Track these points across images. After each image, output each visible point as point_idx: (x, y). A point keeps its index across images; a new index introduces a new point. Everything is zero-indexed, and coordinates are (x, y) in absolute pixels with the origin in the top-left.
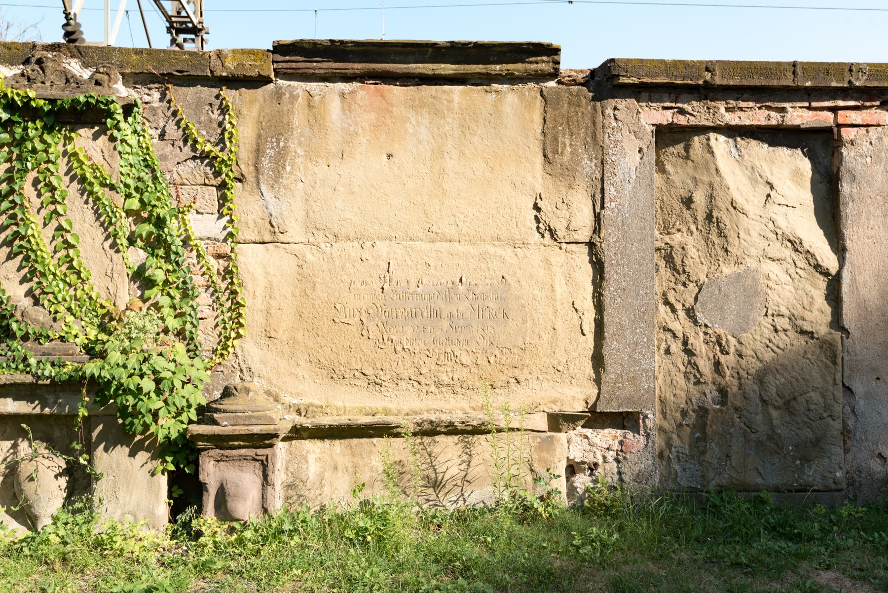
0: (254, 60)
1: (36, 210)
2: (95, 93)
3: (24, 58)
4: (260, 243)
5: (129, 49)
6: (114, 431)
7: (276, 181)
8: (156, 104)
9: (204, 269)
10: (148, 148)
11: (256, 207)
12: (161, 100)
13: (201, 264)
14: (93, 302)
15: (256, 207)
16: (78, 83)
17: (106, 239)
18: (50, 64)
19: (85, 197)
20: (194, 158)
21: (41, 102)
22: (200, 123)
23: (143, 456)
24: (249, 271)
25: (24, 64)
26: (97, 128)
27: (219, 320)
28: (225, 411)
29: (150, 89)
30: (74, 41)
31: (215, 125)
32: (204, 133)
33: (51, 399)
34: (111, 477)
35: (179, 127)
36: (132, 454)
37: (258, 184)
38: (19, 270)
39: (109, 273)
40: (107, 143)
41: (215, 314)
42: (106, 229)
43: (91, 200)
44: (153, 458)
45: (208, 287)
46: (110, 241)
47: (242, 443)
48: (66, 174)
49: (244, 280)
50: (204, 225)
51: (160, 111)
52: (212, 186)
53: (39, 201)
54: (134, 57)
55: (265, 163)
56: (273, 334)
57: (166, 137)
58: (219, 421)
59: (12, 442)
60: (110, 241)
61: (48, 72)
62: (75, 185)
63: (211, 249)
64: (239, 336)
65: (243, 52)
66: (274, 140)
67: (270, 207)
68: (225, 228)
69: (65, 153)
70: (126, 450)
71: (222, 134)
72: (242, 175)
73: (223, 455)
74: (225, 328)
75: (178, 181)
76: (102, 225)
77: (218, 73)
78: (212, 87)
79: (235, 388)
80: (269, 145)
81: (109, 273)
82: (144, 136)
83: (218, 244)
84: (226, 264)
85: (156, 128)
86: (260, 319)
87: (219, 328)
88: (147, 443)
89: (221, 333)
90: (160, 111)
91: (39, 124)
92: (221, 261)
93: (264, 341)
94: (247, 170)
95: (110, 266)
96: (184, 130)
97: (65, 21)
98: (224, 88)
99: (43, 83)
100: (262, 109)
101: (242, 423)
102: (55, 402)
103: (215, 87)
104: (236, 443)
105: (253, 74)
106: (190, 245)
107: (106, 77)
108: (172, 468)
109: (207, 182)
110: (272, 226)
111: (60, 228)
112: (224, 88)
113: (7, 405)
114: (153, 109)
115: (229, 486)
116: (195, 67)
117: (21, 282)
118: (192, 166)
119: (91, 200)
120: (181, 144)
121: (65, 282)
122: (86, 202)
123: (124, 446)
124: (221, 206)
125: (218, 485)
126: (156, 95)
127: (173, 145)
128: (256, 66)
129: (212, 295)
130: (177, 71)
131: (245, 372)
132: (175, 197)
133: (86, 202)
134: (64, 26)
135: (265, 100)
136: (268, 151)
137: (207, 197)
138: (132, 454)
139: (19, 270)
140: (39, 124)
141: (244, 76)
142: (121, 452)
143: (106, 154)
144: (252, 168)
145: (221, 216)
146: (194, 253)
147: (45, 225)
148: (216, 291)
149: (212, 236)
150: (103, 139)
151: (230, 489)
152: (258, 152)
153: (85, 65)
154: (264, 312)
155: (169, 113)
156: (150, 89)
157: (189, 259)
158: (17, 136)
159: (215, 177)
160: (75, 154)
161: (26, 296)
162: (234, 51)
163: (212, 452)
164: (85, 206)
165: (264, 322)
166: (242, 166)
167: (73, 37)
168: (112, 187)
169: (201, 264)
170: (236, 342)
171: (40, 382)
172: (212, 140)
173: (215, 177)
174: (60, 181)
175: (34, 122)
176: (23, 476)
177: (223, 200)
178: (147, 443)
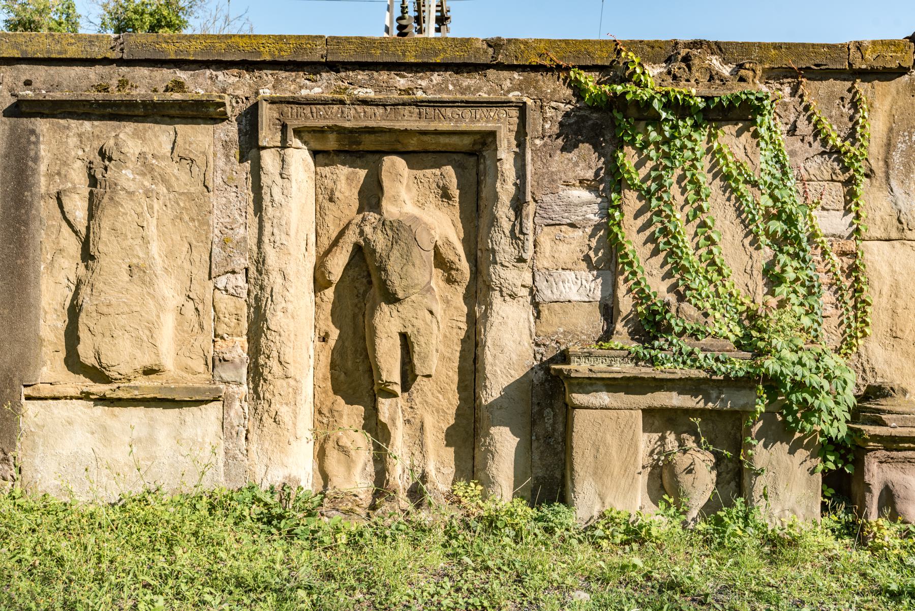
0: (894, 52)
1: (679, 207)
2: (738, 89)
3: (667, 56)
4: (886, 240)
5: (768, 44)
6: (773, 427)
7: (906, 176)
8: (787, 100)
9: (829, 266)
10: (780, 145)
11: (885, 204)
12: (793, 94)
13: (826, 262)
14: (733, 299)
15: (885, 204)
16: (723, 80)
17: (746, 236)
18: (696, 61)
19: (727, 194)
20: (822, 154)
21: (699, 100)
22: (831, 117)
23: (802, 454)
24: (875, 270)
25: (666, 62)
26: (740, 125)
27: (844, 318)
28: (890, 412)
29: (782, 84)
30: (405, 34)
31: (846, 119)
32: (835, 127)
33: (714, 394)
34: (771, 473)
35: (810, 122)
36: (792, 452)
37: (888, 178)
38: (662, 266)
39: (748, 270)
40: (750, 140)
41: (839, 312)
42: (746, 227)
43: (733, 197)
44: (813, 456)
45: (831, 285)
46: (750, 238)
47: (912, 445)
48: (709, 171)
49: (871, 278)
50: (830, 222)
51: (791, 107)
52: (839, 181)
53: (683, 198)
54: (773, 52)
55: (897, 158)
56: (899, 334)
57: (797, 133)
58: (887, 422)
59: (660, 434)
60: (750, 238)
61: (694, 69)
62: (718, 182)
63: (835, 246)
64: (865, 335)
65: (883, 43)
66: (906, 133)
67: (900, 203)
68: (851, 224)
69: (709, 150)
70: (787, 447)
71: (853, 129)
72: (871, 170)
73: (888, 457)
74: (849, 326)
75: (806, 177)
76: (743, 222)
77: (856, 66)
78: (845, 80)
79: (892, 388)
80: (901, 139)
81: (748, 270)
82: (775, 132)
83: (842, 241)
84: (851, 261)
85: (787, 124)
86: (885, 318)
87: (843, 327)
88: (806, 441)
89: (845, 332)
90: (791, 107)
91: (689, 122)
92: (844, 259)
93: (889, 341)
94: (878, 166)
95: (750, 263)
96: (815, 126)
97: (400, 15)
98: (858, 81)
99: (688, 80)
100: (894, 101)
101: (910, 424)
102: (718, 398)
103: (848, 80)
104: (906, 445)
105: (893, 66)
106: (816, 242)
107: (751, 73)
108: (831, 466)
109: (834, 177)
110: (901, 222)
111: (703, 224)
112: (858, 81)
113: (671, 398)
114: (785, 104)
115: (897, 487)
116: (834, 60)
117: (663, 279)
118: (819, 161)
119: (733, 197)
120: (811, 139)
121: (705, 278)
122: (729, 199)
123: (784, 444)
124: (847, 202)
125: (882, 487)
126: (787, 90)
127: (802, 140)
128: (897, 58)
129: (836, 292)
130: (816, 65)
131: (868, 372)
132: (802, 193)
133: (729, 199)
134: (399, 19)
135: (898, 93)
136: (900, 145)
137: (834, 193)
138: (792, 452)
139: (662, 266)
140: (689, 122)
141: (884, 68)
142: (781, 448)
143: (749, 150)
144: (881, 163)
145: (848, 211)
146: (819, 251)
147: (688, 221)
148: (840, 288)
149: (838, 233)
150: (746, 135)
151: (898, 490)
152: (889, 146)
153: (725, 62)
154: (890, 312)
155: (801, 109)
156: (782, 84)
157: (814, 255)
158: (667, 134)
159: (844, 173)
160: (720, 150)
161: (668, 292)
162: (874, 43)
163: (878, 454)
164: (727, 203)
165: (890, 321)
166: (872, 161)
167: (405, 31)
168: (755, 184)
169: (826, 262)
170: (860, 342)
171: (714, 377)
172: (842, 134)
173: (844, 173)
174: (704, 178)
175: (684, 120)
176: (679, 469)
177: (851, 195)
178: (806, 441)
